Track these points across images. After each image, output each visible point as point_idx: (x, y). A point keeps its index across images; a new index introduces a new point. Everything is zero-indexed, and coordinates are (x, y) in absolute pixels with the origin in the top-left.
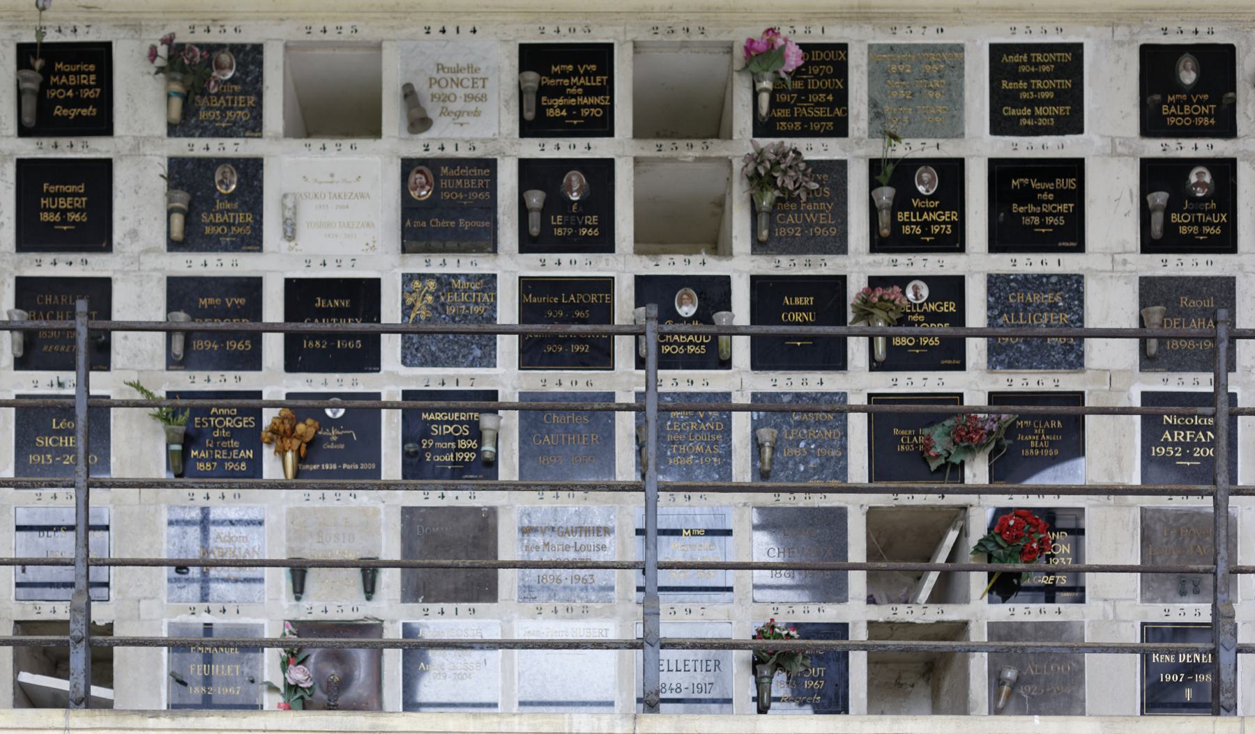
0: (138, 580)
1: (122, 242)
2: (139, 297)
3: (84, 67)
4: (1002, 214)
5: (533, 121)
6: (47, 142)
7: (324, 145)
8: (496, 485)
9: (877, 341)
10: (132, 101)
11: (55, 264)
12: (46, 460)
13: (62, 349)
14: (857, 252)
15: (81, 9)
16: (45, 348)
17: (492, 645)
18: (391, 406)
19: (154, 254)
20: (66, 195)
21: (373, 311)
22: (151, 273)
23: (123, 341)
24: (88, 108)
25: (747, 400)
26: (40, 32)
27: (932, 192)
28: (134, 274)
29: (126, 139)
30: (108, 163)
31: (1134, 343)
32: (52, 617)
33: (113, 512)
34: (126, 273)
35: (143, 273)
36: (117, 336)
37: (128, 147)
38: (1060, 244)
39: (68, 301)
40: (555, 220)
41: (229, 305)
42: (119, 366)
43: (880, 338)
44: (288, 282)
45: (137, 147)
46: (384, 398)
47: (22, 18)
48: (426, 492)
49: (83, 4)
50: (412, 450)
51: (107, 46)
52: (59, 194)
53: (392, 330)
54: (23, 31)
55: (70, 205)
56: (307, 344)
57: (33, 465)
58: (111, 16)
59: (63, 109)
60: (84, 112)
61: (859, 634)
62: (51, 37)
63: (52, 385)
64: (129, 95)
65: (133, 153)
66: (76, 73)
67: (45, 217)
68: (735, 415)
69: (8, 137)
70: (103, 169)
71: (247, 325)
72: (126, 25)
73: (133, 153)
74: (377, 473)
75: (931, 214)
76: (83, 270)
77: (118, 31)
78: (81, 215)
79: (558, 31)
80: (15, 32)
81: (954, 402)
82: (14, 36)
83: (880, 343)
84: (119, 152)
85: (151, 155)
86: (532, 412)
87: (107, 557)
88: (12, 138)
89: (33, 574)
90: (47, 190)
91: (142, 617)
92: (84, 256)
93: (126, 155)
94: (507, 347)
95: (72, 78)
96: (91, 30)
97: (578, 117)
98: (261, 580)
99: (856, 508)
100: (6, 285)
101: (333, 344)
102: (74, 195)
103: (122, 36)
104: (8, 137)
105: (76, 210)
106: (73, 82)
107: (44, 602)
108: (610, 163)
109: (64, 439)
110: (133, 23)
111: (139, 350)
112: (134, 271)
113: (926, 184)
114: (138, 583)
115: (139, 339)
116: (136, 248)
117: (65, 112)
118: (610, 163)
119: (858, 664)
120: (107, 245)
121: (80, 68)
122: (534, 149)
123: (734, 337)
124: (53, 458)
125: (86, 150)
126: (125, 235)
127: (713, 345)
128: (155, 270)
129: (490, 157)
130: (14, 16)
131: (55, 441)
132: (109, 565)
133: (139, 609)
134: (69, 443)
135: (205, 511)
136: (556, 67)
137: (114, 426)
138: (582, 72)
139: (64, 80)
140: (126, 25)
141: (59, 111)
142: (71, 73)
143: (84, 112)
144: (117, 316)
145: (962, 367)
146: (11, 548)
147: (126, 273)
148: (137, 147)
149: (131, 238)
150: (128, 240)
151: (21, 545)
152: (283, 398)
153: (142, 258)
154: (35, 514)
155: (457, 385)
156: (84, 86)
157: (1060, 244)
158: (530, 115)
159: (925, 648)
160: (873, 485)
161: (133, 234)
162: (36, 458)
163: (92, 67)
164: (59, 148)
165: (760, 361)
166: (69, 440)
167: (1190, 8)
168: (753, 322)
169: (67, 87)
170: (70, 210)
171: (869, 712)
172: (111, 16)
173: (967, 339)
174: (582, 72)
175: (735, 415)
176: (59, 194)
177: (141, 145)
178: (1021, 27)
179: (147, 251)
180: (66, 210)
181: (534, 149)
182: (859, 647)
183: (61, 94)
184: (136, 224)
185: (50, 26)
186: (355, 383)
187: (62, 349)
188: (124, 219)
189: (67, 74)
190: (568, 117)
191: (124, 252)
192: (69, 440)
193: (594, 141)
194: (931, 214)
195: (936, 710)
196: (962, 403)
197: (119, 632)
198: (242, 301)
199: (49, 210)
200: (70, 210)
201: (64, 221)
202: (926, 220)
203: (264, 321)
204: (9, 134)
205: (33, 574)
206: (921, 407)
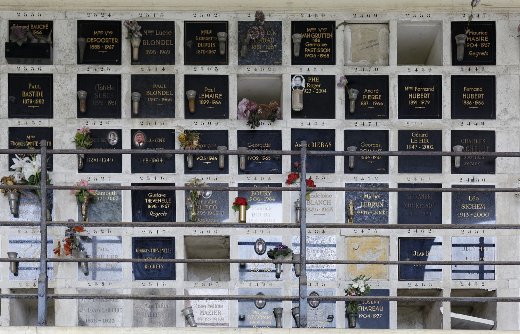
0: (508, 270)
1: (500, 115)
2: (508, 140)
3: (482, 33)
6: (466, 68)
7: (469, 68)
10: (505, 49)
11: (470, 124)
12: (466, 215)
13: (473, 164)
15: (483, 6)
16: (465, 163)
17: (69, 297)
18: (393, 190)
19: (515, 120)
20: (474, 93)
21: (386, 147)
22: (513, 129)
23: (501, 160)
24: (484, 52)
26: (471, 16)
28: (506, 129)
29: (502, 67)
30: (494, 77)
32: (469, 287)
33: (496, 239)
34: (502, 129)
35: (510, 129)
36: (498, 160)
37: (503, 70)
39: (475, 141)
40: (200, 96)
41: (106, 34)
42: (499, 172)
44: (239, 132)
45: (507, 70)
46: (390, 187)
47: (455, 10)
48: (409, 229)
49: (484, 3)
50: (350, 208)
51: (493, 23)
52: (471, 92)
54: (454, 16)
55: (476, 97)
56: (198, 51)
57: (460, 217)
58: (496, 9)
59: (473, 52)
60: (483, 54)
61: (393, 294)
62: (475, 19)
63: (469, 181)
64: (503, 46)
65: (505, 73)
66: (478, 36)
67: (465, 102)
68: (230, 192)
69: (447, 65)
70: (491, 80)
72: (502, 14)
73: (505, 73)
74: (174, 220)
76: (482, 127)
77: (498, 16)
78: (481, 102)
80: (451, 16)
82: (450, 18)
83: (458, 159)
84: (498, 73)
85: (513, 74)
87: (494, 261)
88: (450, 66)
89: (459, 267)
90: (466, 90)
91: (510, 287)
92: (483, 121)
93: (502, 74)
95: (477, 38)
96: (486, 16)
98: (120, 270)
100: (447, 134)
101: (100, 160)
102: (478, 92)
103: (500, 18)
104: (447, 65)
105: (479, 100)
106: (477, 40)
107: (465, 281)
108: (226, 77)
109: (474, 205)
110: (505, 13)
111: (508, 165)
112: (506, 128)
114: (508, 272)
115: (508, 160)
116: (507, 117)
117: (474, 54)
118: (226, 77)
119: (393, 306)
120: (493, 116)
121: (480, 33)
124: (469, 214)
125: (483, 72)
126: (501, 111)
128: (515, 127)
129: (386, 75)
130: (451, 9)
131: (470, 207)
132: (495, 265)
133: (508, 284)
134: (476, 207)
135: (482, 239)
136: (96, 32)
137: (497, 199)
138: (320, 31)
139: (473, 39)
140: (502, 14)
142: (476, 36)
143: (483, 54)
144: (498, 149)
146: (450, 256)
147: (502, 129)
148: (507, 70)
149: (504, 113)
150: (503, 114)
151: (454, 254)
152: (130, 185)
153: (509, 122)
154: (461, 240)
156: (482, 42)
158: (297, 54)
161: (505, 111)
162: (462, 214)
163: (486, 33)
164: (471, 71)
165: (402, 169)
166: (476, 206)
169: (474, 42)
170: (476, 100)
171: (398, 328)
172: (496, 9)
174: (320, 31)
175: (230, 192)
176: (471, 92)
177: (509, 70)
179: (511, 119)
180: (474, 100)
182: (393, 299)
183: (472, 45)
184: (507, 106)
185: (467, 14)
187: (473, 164)
188: (501, 103)
189: (475, 36)
191: (501, 119)
192: (476, 206)
193: (166, 66)
195: (425, 327)
197: (499, 295)
199: (467, 100)
200: (476, 100)
201: (103, 49)
204: (448, 64)
205: (459, 267)
206: (408, 189)
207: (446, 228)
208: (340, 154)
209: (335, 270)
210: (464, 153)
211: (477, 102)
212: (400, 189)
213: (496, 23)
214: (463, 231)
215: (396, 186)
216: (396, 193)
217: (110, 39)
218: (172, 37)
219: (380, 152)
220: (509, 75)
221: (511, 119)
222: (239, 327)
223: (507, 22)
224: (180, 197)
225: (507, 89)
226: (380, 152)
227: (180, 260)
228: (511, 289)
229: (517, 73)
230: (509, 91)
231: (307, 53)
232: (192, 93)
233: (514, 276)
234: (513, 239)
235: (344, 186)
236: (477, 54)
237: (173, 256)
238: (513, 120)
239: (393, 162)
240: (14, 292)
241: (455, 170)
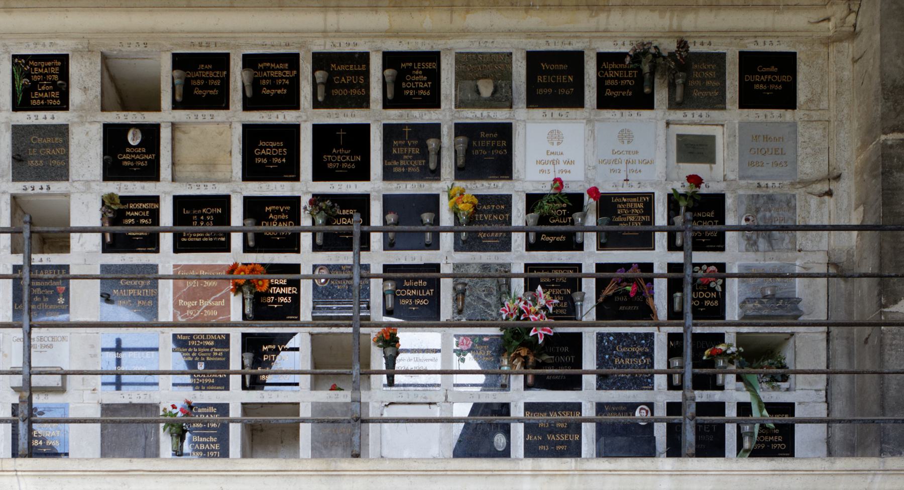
5: (251, 98)
8: (580, 324)
21: (225, 218)
24: (213, 90)
27: (139, 141)
31: (99, 235)
60: (279, 92)
71: (504, 227)
86: (487, 279)
98: (157, 384)
99: (236, 336)
113: (134, 138)
123: (585, 233)
127: (571, 235)
135: (119, 341)
141: (197, 92)
143: (279, 92)
157: (708, 246)
159: (612, 421)
160: (671, 321)
165: (389, 245)
167: (774, 31)
168: (175, 224)
178: (620, 42)
182: (519, 420)
196: (580, 271)
201: (270, 163)
202: (263, 154)
203: (301, 225)
208: (661, 230)
209: (297, 384)
210: (329, 228)
211: (275, 160)
212: (672, 275)
218: (366, 74)
219: (716, 227)
226: (716, 227)
231: (406, 89)
232: (320, 75)
236: (616, 94)
237: (579, 366)
239: (166, 241)
241: (316, 248)
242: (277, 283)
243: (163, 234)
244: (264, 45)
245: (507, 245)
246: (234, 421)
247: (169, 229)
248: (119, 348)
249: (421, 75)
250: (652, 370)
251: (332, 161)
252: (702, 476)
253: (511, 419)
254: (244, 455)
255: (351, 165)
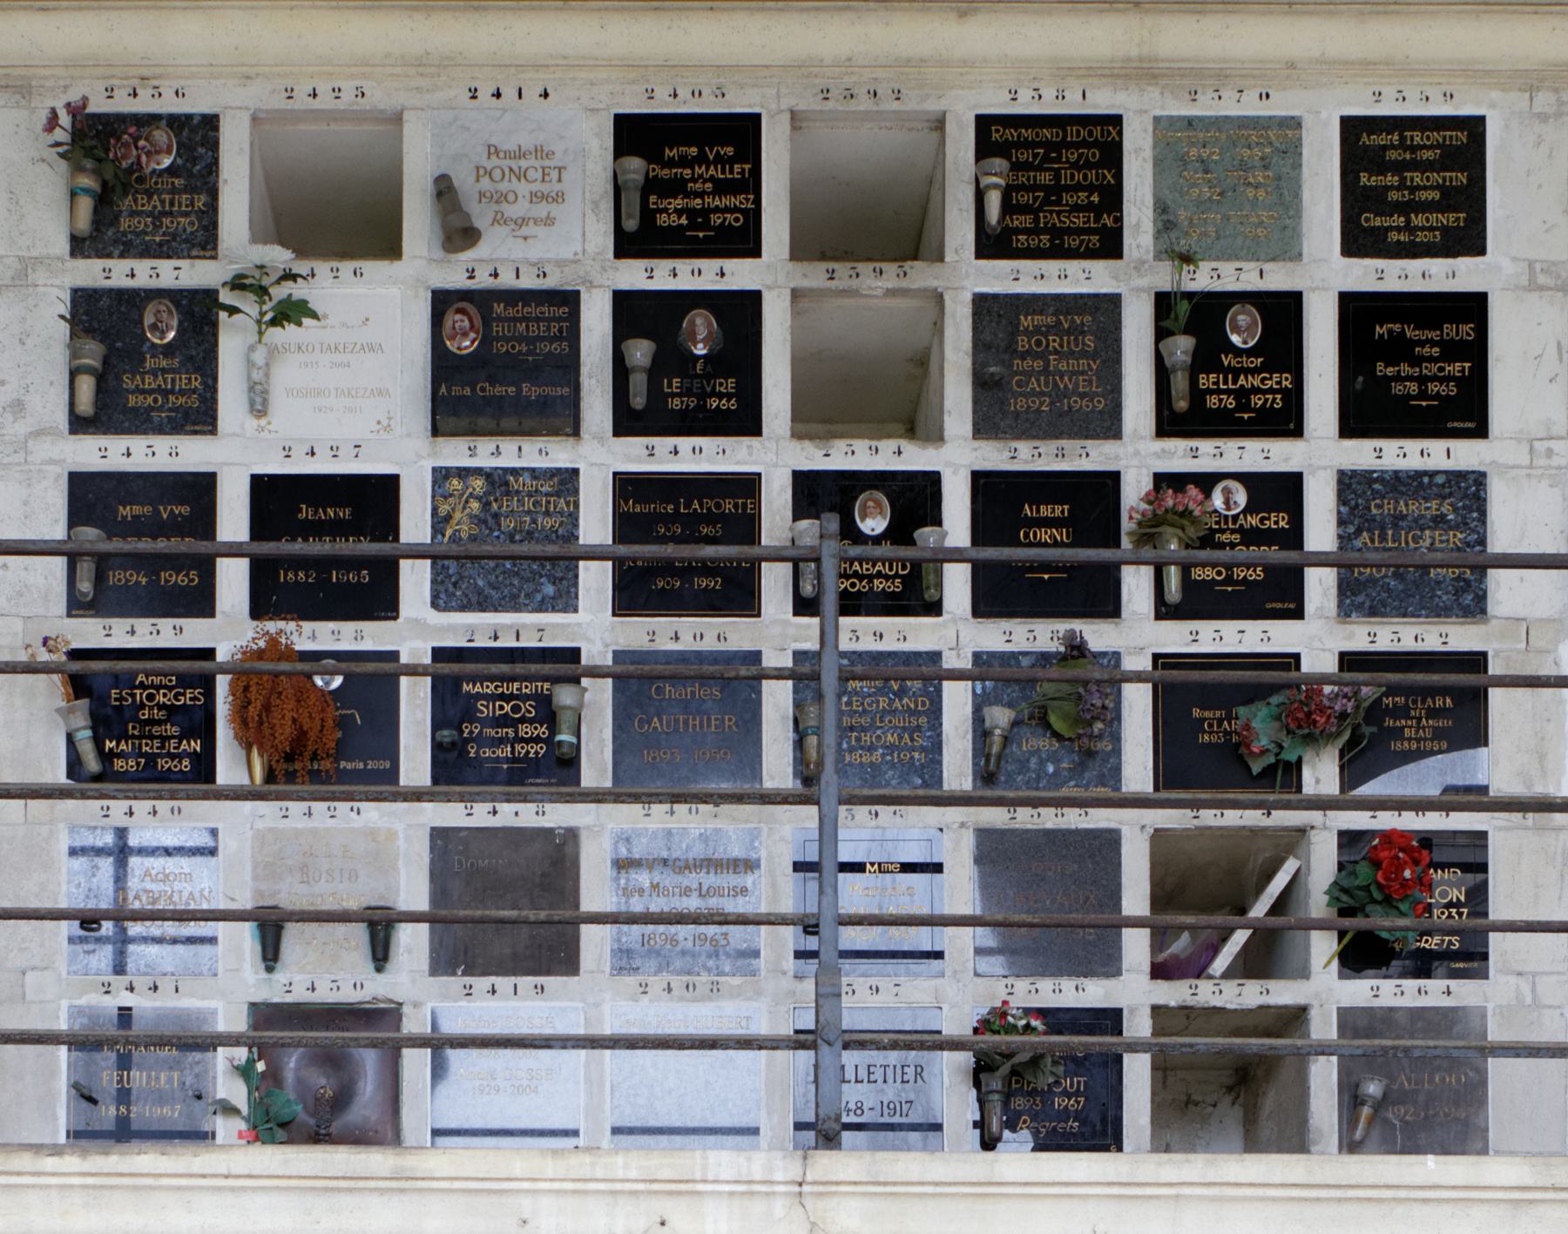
0: (23, 940)
2: (26, 503)
4: (1361, 379)
5: (637, 231)
9: (1168, 574)
14: (1137, 436)
19: (49, 438)
21: (747, 527)
25: (966, 663)
28: (19, 468)
29: (6, 261)
35: (32, 467)
38: (1269, 606)
41: (165, 516)
43: (1173, 567)
46: (404, 659)
53: (416, 553)
72: (7, 87)
74: (392, 775)
75: (1250, 378)
79: (675, 95)
81: (1286, 667)
85: (45, 285)
91: (28, 998)
94: (595, 580)
97: (706, 226)
98: (212, 940)
110: (19, 83)
112: (19, 464)
119: (1137, 1074)
122: (637, 275)
128: (52, 462)
133: (23, 986)
140: (7, 87)
145: (1298, 614)
153: (30, 443)
155: (518, 639)
157: (1269, 606)
158: (631, 225)
159: (1255, 1049)
160: (1164, 795)
173: (219, 561)
174: (711, 157)
177: (30, 271)
179: (38, 433)
181: (637, 275)
186: (359, 637)
190: (1236, 410)
194: (1250, 378)
198: (184, 510)
203: (1306, 549)
207: (227, 798)
213: (621, 111)
214: (108, 808)
215: (788, 662)
216: (428, 681)
217: (1032, 174)
220: (31, 289)
221: (38, 433)
222: (76, 1135)
223: (26, 113)
224: (777, 699)
225: (23, 337)
227: (1560, 922)
228: (33, 1002)
229: (57, 282)
230: (29, 342)
233: (42, 960)
234: (39, 834)
235: (789, 664)
238: (44, 438)
239: (1320, 585)
240: (1357, 1034)
242: (528, 691)
243: (410, 561)
244: (750, 106)
245: (479, 604)
246: (1135, 1047)
247: (55, 546)
248: (122, 852)
249: (708, 194)
250: (570, 550)
251: (1402, 380)
252: (255, 1172)
253: (402, 1039)
254: (1162, 1143)
255: (728, 401)
